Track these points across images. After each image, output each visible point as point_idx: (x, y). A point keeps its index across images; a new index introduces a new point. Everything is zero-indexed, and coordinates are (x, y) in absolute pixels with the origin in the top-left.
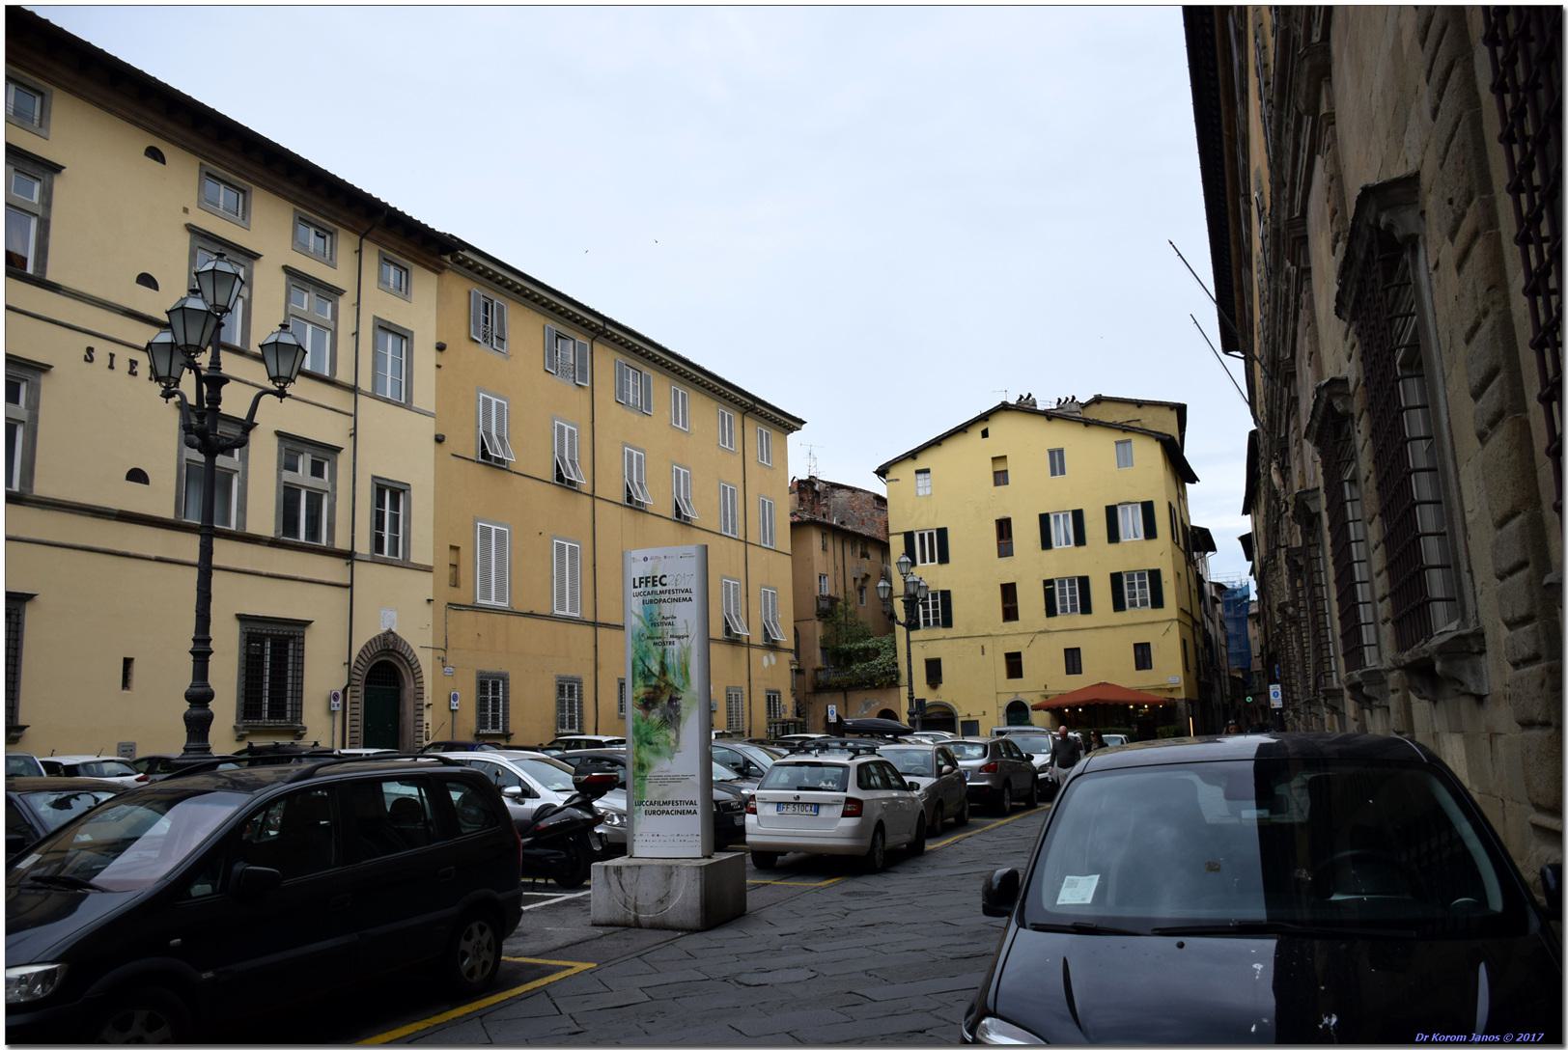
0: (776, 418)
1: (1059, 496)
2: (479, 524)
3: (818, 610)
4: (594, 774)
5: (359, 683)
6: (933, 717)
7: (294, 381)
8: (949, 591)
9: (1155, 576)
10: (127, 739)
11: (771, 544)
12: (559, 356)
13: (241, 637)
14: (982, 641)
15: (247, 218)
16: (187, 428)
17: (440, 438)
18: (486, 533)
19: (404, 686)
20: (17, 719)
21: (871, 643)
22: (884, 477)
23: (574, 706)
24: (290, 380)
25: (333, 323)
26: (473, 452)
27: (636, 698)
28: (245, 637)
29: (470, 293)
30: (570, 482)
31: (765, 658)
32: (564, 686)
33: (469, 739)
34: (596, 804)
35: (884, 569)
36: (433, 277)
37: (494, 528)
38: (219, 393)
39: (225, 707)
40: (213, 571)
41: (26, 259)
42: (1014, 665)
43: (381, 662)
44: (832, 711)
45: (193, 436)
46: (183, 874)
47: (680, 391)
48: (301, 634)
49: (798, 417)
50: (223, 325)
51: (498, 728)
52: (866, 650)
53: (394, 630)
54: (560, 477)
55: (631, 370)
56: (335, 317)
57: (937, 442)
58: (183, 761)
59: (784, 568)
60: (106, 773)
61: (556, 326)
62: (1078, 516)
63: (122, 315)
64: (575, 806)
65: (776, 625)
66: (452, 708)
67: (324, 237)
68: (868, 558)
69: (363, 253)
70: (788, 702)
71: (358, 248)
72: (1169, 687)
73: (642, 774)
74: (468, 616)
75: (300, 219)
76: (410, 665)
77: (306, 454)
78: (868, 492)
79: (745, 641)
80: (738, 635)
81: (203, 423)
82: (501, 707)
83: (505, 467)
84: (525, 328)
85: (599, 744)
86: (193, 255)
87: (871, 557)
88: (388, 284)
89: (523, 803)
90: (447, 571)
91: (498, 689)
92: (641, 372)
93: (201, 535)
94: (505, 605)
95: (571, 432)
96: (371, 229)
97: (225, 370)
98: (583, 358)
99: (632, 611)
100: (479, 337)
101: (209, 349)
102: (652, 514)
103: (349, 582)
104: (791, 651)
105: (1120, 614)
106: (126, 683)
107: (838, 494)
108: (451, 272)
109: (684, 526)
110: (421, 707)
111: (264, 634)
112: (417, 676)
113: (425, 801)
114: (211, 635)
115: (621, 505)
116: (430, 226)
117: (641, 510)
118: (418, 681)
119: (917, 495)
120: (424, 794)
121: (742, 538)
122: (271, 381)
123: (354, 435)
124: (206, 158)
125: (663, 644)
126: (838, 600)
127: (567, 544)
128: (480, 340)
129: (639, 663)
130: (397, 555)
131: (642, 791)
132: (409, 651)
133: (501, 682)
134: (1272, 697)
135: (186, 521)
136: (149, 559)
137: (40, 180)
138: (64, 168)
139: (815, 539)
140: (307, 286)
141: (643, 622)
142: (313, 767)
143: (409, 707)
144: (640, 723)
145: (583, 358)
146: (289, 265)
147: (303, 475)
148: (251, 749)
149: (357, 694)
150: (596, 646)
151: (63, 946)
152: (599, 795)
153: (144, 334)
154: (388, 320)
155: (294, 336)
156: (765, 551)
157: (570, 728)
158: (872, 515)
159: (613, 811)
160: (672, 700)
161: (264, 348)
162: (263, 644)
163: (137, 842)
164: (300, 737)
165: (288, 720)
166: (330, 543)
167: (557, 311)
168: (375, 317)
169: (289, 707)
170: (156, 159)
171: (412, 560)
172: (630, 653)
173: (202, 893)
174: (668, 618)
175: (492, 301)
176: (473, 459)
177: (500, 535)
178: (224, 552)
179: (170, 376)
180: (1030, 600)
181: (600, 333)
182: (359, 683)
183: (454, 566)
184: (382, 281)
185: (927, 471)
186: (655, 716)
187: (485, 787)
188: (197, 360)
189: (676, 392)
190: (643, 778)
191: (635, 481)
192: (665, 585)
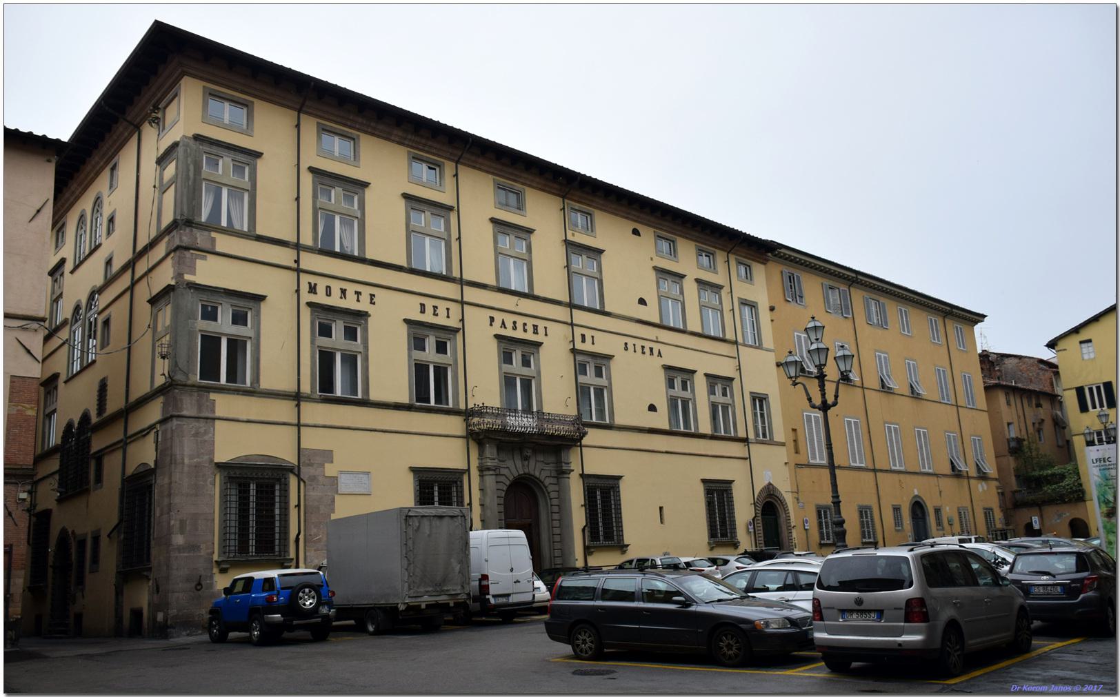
0: (932, 305)
3: (1010, 448)
11: (973, 405)
19: (780, 516)
21: (1057, 469)
22: (1054, 349)
25: (681, 296)
29: (782, 272)
31: (980, 485)
35: (1054, 414)
44: (1035, 521)
49: (981, 313)
52: (1053, 475)
56: (721, 303)
57: (1096, 319)
59: (983, 420)
61: (827, 282)
65: (983, 462)
68: (1041, 407)
70: (998, 515)
74: (806, 471)
75: (699, 250)
78: (1033, 358)
79: (965, 474)
80: (960, 471)
84: (812, 286)
86: (658, 283)
87: (1043, 406)
90: (792, 444)
98: (845, 299)
99: (1094, 475)
102: (898, 394)
104: (996, 479)
106: (662, 522)
107: (1007, 361)
114: (839, 494)
115: (908, 396)
116: (752, 235)
117: (891, 393)
119: (1083, 359)
121: (954, 403)
124: (657, 228)
126: (1024, 440)
129: (1101, 497)
130: (766, 437)
136: (662, 452)
139: (1001, 397)
143: (784, 528)
145: (845, 299)
146: (495, 217)
150: (877, 485)
156: (970, 411)
158: (1038, 374)
165: (276, 554)
175: (793, 274)
181: (853, 282)
185: (1090, 341)
191: (885, 374)
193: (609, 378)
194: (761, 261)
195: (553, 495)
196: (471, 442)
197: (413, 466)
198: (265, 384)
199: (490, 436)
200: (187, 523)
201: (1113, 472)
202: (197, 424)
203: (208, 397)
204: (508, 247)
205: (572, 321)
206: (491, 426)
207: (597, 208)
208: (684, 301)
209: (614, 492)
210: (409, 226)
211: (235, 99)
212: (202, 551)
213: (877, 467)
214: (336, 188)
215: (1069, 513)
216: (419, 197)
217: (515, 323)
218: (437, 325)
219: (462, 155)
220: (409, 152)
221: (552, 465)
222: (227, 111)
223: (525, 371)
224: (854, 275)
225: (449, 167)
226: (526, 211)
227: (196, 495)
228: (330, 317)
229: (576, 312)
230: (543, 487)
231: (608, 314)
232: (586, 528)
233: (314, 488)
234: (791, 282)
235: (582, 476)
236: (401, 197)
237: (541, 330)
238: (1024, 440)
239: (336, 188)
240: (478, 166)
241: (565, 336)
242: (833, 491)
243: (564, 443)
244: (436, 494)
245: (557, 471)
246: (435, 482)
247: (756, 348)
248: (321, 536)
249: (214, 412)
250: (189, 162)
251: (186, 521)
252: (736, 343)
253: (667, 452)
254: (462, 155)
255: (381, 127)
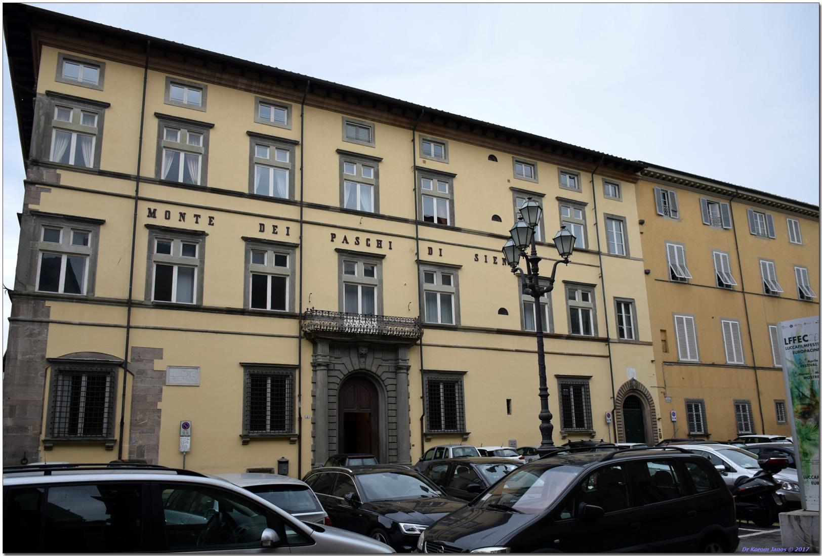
2: (675, 316)
4: (771, 459)
5: (619, 408)
7: (571, 254)
10: (513, 438)
12: (711, 214)
13: (558, 386)
15: (536, 178)
16: (525, 286)
17: (647, 272)
18: (680, 321)
20: (466, 429)
23: (747, 418)
24: (570, 254)
25: (584, 221)
26: (667, 276)
27: (796, 412)
28: (560, 386)
29: (654, 190)
30: (728, 286)
32: (739, 406)
33: (685, 437)
34: (775, 476)
36: (631, 187)
37: (684, 317)
38: (537, 266)
39: (556, 422)
40: (545, 355)
41: (446, 219)
43: (631, 396)
45: (528, 289)
46: (556, 507)
47: (793, 221)
48: (587, 383)
50: (535, 232)
51: (701, 431)
53: (635, 378)
54: (721, 284)
55: (758, 214)
56: (584, 218)
58: (542, 450)
60: (506, 455)
61: (705, 198)
63: (488, 236)
64: (761, 478)
66: (673, 420)
67: (574, 178)
69: (595, 182)
71: (591, 180)
73: (806, 459)
74: (676, 368)
76: (646, 397)
77: (269, 252)
81: (532, 282)
82: (701, 419)
83: (686, 282)
85: (767, 440)
86: (514, 201)
88: (609, 195)
89: (727, 475)
90: (660, 344)
91: (698, 408)
92: (764, 214)
93: (537, 337)
94: (696, 360)
95: (724, 257)
96: (597, 168)
97: (539, 255)
98: (725, 212)
99: (786, 359)
100: (662, 212)
101: (530, 246)
102: (693, 285)
103: (608, 354)
106: (509, 412)
108: (642, 181)
109: (807, 303)
110: (655, 420)
111: (570, 384)
112: (651, 403)
113: (674, 473)
114: (548, 386)
115: (797, 300)
116: (627, 159)
117: (686, 284)
118: (651, 405)
120: (673, 470)
122: (561, 256)
123: (602, 277)
127: (730, 322)
128: (663, 215)
130: (632, 338)
131: (808, 470)
132: (645, 389)
133: (700, 404)
135: (526, 330)
136: (512, 351)
137: (448, 183)
138: (456, 175)
140: (570, 205)
141: (795, 365)
142: (612, 453)
144: (801, 427)
145: (725, 212)
147: (578, 302)
148: (570, 443)
149: (619, 414)
150: (757, 381)
151: (507, 539)
152: (777, 471)
153: (500, 244)
154: (611, 213)
155: (569, 231)
157: (698, 431)
159: (787, 481)
161: (555, 240)
162: (569, 389)
163: (529, 489)
164: (593, 437)
166: (596, 335)
167: (661, 178)
168: (604, 213)
169: (585, 422)
170: (493, 160)
171: (641, 340)
172: (788, 385)
173: (566, 517)
174: (813, 361)
175: (667, 191)
176: (668, 280)
177: (688, 321)
178: (549, 345)
179: (514, 262)
181: (734, 196)
182: (619, 408)
183: (664, 341)
184: (606, 194)
187: (705, 464)
188: (526, 252)
189: (790, 222)
190: (808, 462)
191: (770, 280)
192: (807, 341)
193: (457, 286)
194: (631, 180)
196: (304, 341)
197: (242, 362)
198: (99, 293)
199: (320, 336)
200: (17, 408)
201: (811, 356)
202: (31, 327)
203: (44, 304)
204: (355, 174)
205: (417, 236)
206: (403, 334)
207: (450, 138)
208: (586, 224)
210: (253, 158)
211: (88, 62)
212: (29, 431)
213: (757, 365)
214: (181, 129)
216: (262, 134)
217: (357, 238)
218: (274, 241)
219: (305, 97)
220: (256, 98)
221: (390, 362)
222: (186, 95)
223: (368, 280)
224: (734, 190)
225: (296, 109)
226: (375, 143)
227: (27, 385)
228: (168, 237)
229: (142, 186)
230: (381, 381)
231: (458, 230)
232: (424, 417)
233: (142, 381)
234: (665, 199)
235: (424, 372)
236: (509, 190)
237: (385, 244)
239: (181, 129)
240: (325, 106)
241: (411, 249)
242: (541, 385)
243: (400, 342)
244: (269, 386)
245: (395, 367)
246: (269, 376)
247: (623, 257)
248: (146, 421)
249: (49, 317)
250: (40, 114)
251: (16, 406)
252: (598, 253)
253: (517, 351)
254: (305, 97)
255: (225, 77)
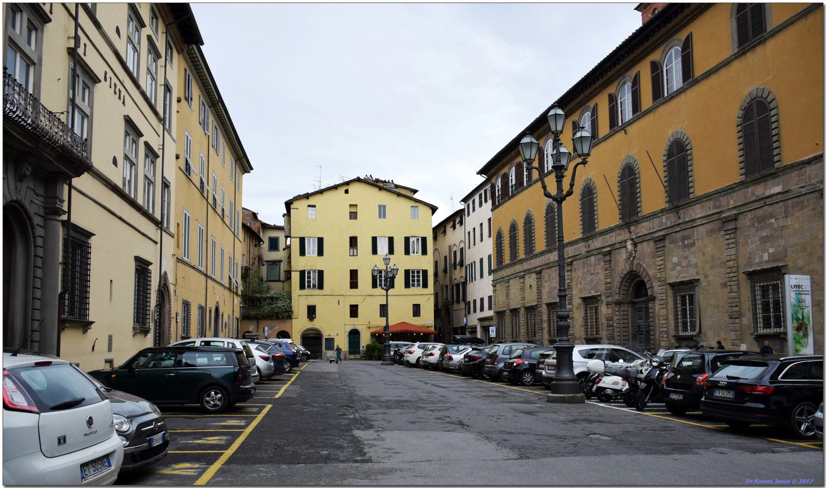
1: (383, 230)
6: (311, 336)
8: (323, 271)
9: (425, 272)
14: (339, 298)
42: (354, 311)
62: (391, 240)
72: (427, 325)
105: (407, 289)
119: (308, 219)
125: (803, 309)
134: (491, 332)
143: (167, 318)
144: (796, 336)
150: (206, 288)
160: (806, 328)
180: (365, 279)
185: (314, 206)
186: (801, 334)
195: (40, 242)
209: (82, 251)
215: (279, 326)
238: (250, 270)
245: (45, 208)
